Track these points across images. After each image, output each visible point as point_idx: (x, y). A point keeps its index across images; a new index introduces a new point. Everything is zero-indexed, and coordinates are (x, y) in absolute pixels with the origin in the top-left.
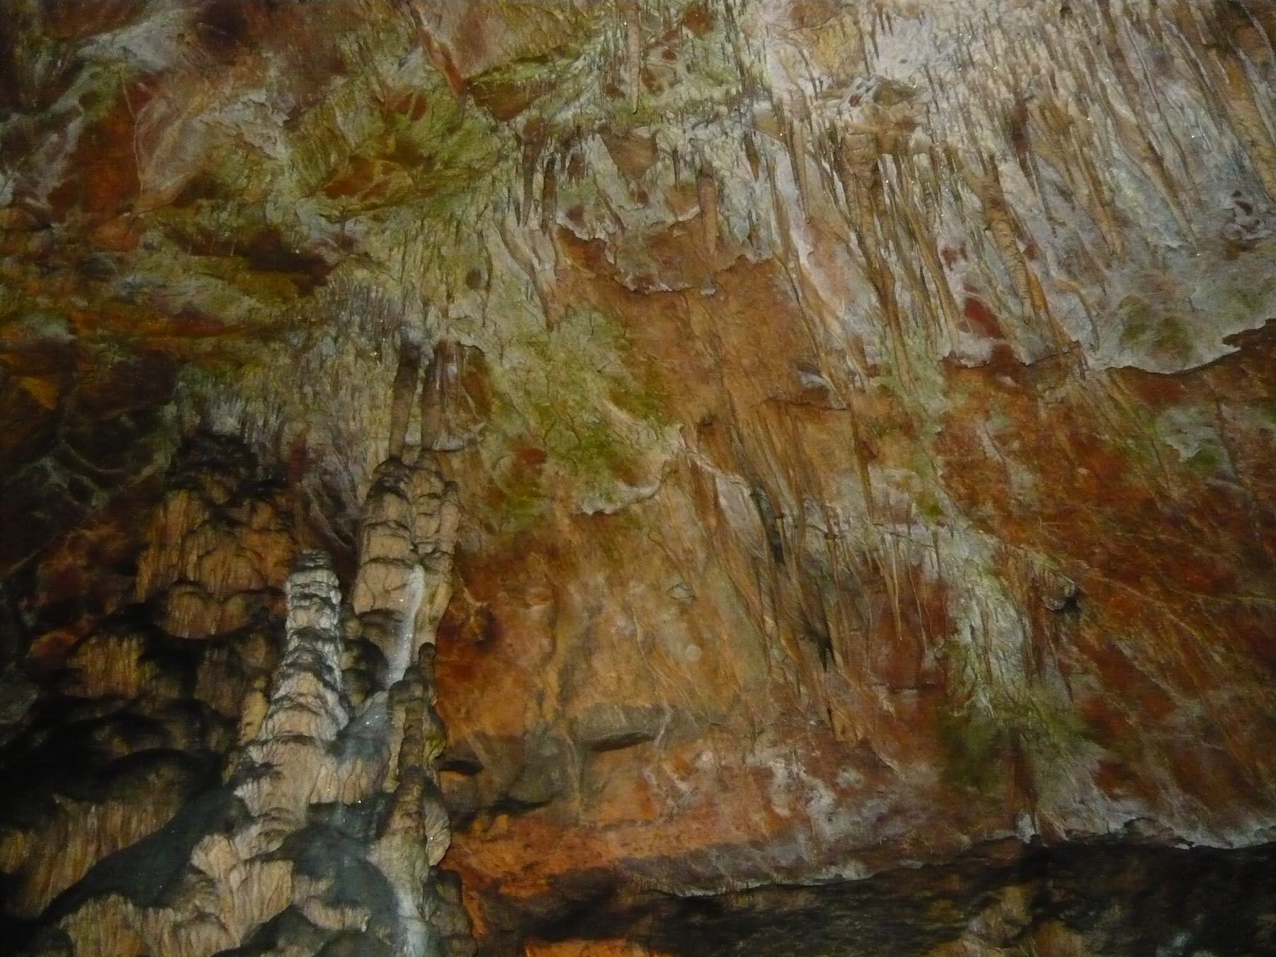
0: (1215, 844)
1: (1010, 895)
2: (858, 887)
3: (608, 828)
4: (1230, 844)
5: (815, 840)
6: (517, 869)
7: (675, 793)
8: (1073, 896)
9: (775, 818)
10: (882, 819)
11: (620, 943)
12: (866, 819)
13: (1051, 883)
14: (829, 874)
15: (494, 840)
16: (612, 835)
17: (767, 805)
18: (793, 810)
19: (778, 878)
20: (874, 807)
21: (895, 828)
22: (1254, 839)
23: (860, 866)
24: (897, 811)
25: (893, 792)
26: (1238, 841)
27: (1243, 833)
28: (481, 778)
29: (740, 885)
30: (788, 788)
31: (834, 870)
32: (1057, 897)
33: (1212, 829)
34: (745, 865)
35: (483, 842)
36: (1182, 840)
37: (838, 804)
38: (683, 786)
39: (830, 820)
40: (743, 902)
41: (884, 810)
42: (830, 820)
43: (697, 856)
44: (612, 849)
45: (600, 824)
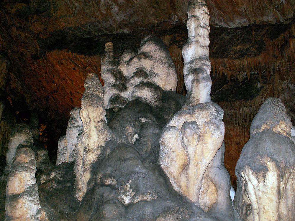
0: (226, 26)
1: (166, 38)
2: (128, 35)
3: (60, 18)
4: (231, 26)
5: (114, 20)
6: (42, 30)
7: (76, 7)
8: (183, 39)
9: (102, 14)
10: (132, 15)
11: (66, 50)
12: (128, 15)
13: (177, 35)
14: (120, 31)
15: (34, 22)
16: (61, 20)
17: (100, 10)
18: (107, 12)
19: (106, 32)
20: (129, 11)
21: (135, 18)
22: (238, 26)
23: (128, 29)
24: (135, 12)
25: (134, 6)
26: (233, 26)
27: (234, 23)
28: (31, 5)
29: (96, 34)
30: (105, 5)
31: (121, 30)
32: (178, 39)
33: (226, 22)
34: (97, 28)
35: (32, 23)
36: (217, 25)
37: (119, 10)
38: (76, 5)
39: (118, 15)
40: (97, 39)
41: (132, 12)
42: (118, 15)
43: (84, 25)
44: (62, 24)
45: (58, 17)
